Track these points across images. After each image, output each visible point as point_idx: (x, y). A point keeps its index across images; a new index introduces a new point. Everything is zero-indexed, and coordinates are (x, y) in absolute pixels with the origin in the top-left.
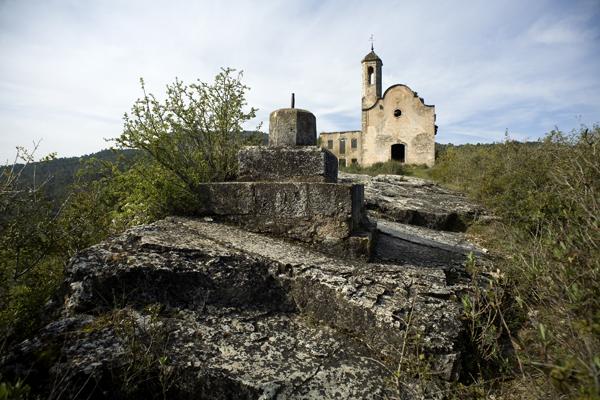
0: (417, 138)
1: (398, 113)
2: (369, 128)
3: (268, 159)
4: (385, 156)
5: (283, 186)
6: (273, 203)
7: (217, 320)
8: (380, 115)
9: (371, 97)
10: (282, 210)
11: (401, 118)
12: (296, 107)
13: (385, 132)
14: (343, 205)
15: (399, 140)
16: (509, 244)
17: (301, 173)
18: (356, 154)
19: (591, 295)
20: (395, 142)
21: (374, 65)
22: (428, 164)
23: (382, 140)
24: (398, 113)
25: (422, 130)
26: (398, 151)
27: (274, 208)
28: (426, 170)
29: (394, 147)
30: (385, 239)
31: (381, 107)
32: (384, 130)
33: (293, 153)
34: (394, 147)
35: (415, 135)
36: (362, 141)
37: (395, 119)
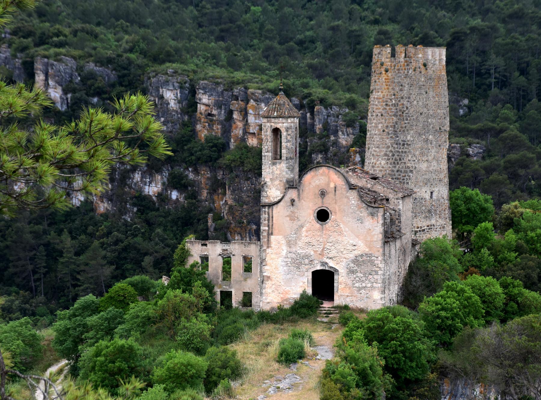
0: (356, 261)
1: (323, 216)
2: (272, 238)
7: (432, 367)
9: (277, 182)
11: (329, 223)
13: (300, 249)
15: (324, 264)
16: (386, 79)
18: (249, 285)
19: (353, 204)
20: (319, 268)
23: (297, 263)
24: (323, 216)
25: (362, 248)
26: (323, 282)
29: (316, 275)
32: (300, 243)
34: (316, 275)
35: (352, 256)
36: (263, 262)
37: (317, 225)
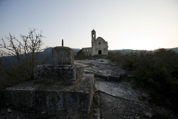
1: (100, 43)
3: (48, 72)
4: (97, 53)
5: (50, 92)
6: (45, 102)
8: (96, 44)
10: (51, 106)
11: (100, 44)
12: (64, 46)
14: (84, 104)
17: (64, 79)
20: (99, 50)
21: (93, 32)
22: (107, 55)
23: (96, 49)
24: (100, 43)
26: (100, 52)
27: (46, 105)
28: (106, 56)
29: (99, 51)
30: (103, 95)
31: (96, 42)
33: (59, 70)
34: (99, 51)
37: (99, 45)
